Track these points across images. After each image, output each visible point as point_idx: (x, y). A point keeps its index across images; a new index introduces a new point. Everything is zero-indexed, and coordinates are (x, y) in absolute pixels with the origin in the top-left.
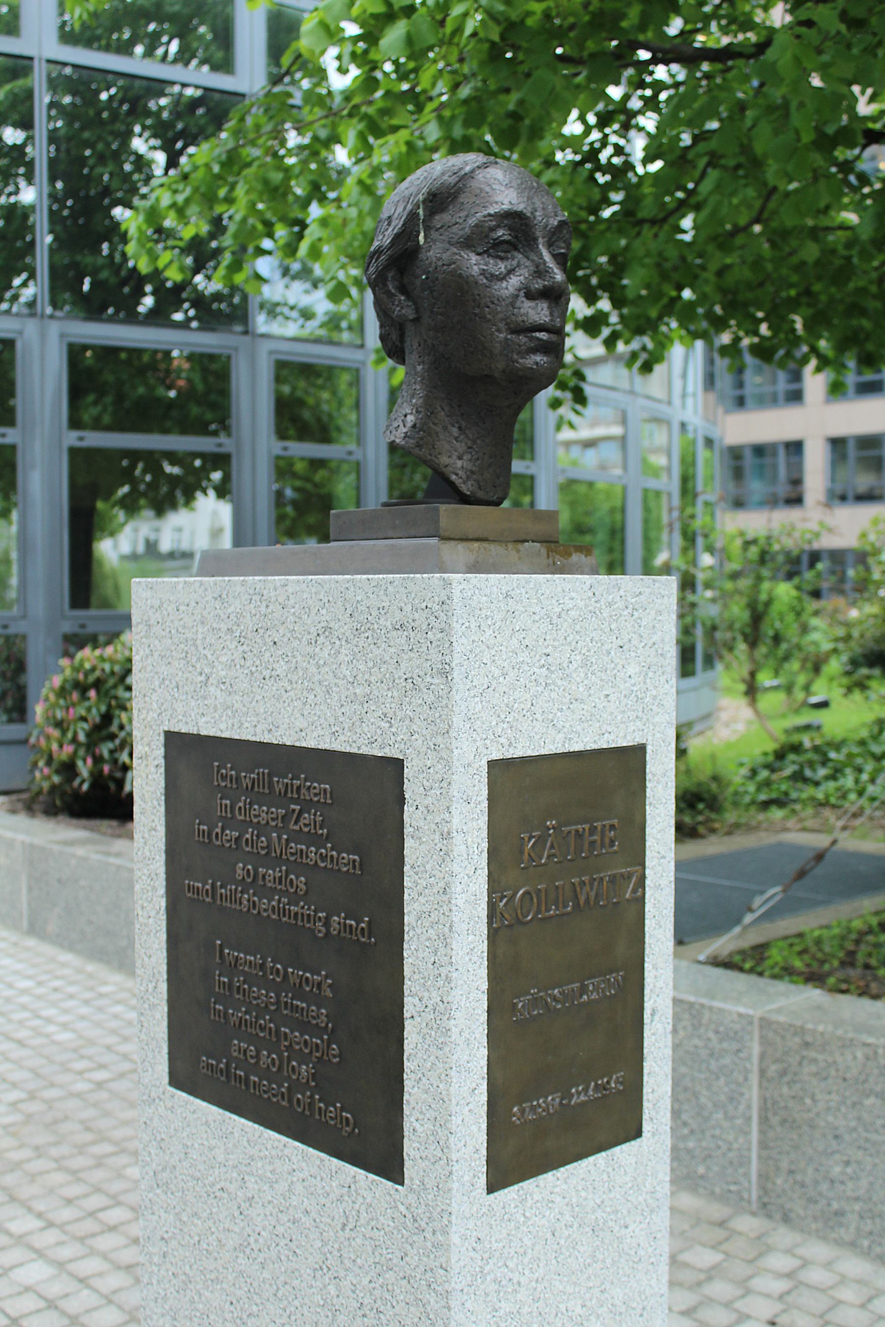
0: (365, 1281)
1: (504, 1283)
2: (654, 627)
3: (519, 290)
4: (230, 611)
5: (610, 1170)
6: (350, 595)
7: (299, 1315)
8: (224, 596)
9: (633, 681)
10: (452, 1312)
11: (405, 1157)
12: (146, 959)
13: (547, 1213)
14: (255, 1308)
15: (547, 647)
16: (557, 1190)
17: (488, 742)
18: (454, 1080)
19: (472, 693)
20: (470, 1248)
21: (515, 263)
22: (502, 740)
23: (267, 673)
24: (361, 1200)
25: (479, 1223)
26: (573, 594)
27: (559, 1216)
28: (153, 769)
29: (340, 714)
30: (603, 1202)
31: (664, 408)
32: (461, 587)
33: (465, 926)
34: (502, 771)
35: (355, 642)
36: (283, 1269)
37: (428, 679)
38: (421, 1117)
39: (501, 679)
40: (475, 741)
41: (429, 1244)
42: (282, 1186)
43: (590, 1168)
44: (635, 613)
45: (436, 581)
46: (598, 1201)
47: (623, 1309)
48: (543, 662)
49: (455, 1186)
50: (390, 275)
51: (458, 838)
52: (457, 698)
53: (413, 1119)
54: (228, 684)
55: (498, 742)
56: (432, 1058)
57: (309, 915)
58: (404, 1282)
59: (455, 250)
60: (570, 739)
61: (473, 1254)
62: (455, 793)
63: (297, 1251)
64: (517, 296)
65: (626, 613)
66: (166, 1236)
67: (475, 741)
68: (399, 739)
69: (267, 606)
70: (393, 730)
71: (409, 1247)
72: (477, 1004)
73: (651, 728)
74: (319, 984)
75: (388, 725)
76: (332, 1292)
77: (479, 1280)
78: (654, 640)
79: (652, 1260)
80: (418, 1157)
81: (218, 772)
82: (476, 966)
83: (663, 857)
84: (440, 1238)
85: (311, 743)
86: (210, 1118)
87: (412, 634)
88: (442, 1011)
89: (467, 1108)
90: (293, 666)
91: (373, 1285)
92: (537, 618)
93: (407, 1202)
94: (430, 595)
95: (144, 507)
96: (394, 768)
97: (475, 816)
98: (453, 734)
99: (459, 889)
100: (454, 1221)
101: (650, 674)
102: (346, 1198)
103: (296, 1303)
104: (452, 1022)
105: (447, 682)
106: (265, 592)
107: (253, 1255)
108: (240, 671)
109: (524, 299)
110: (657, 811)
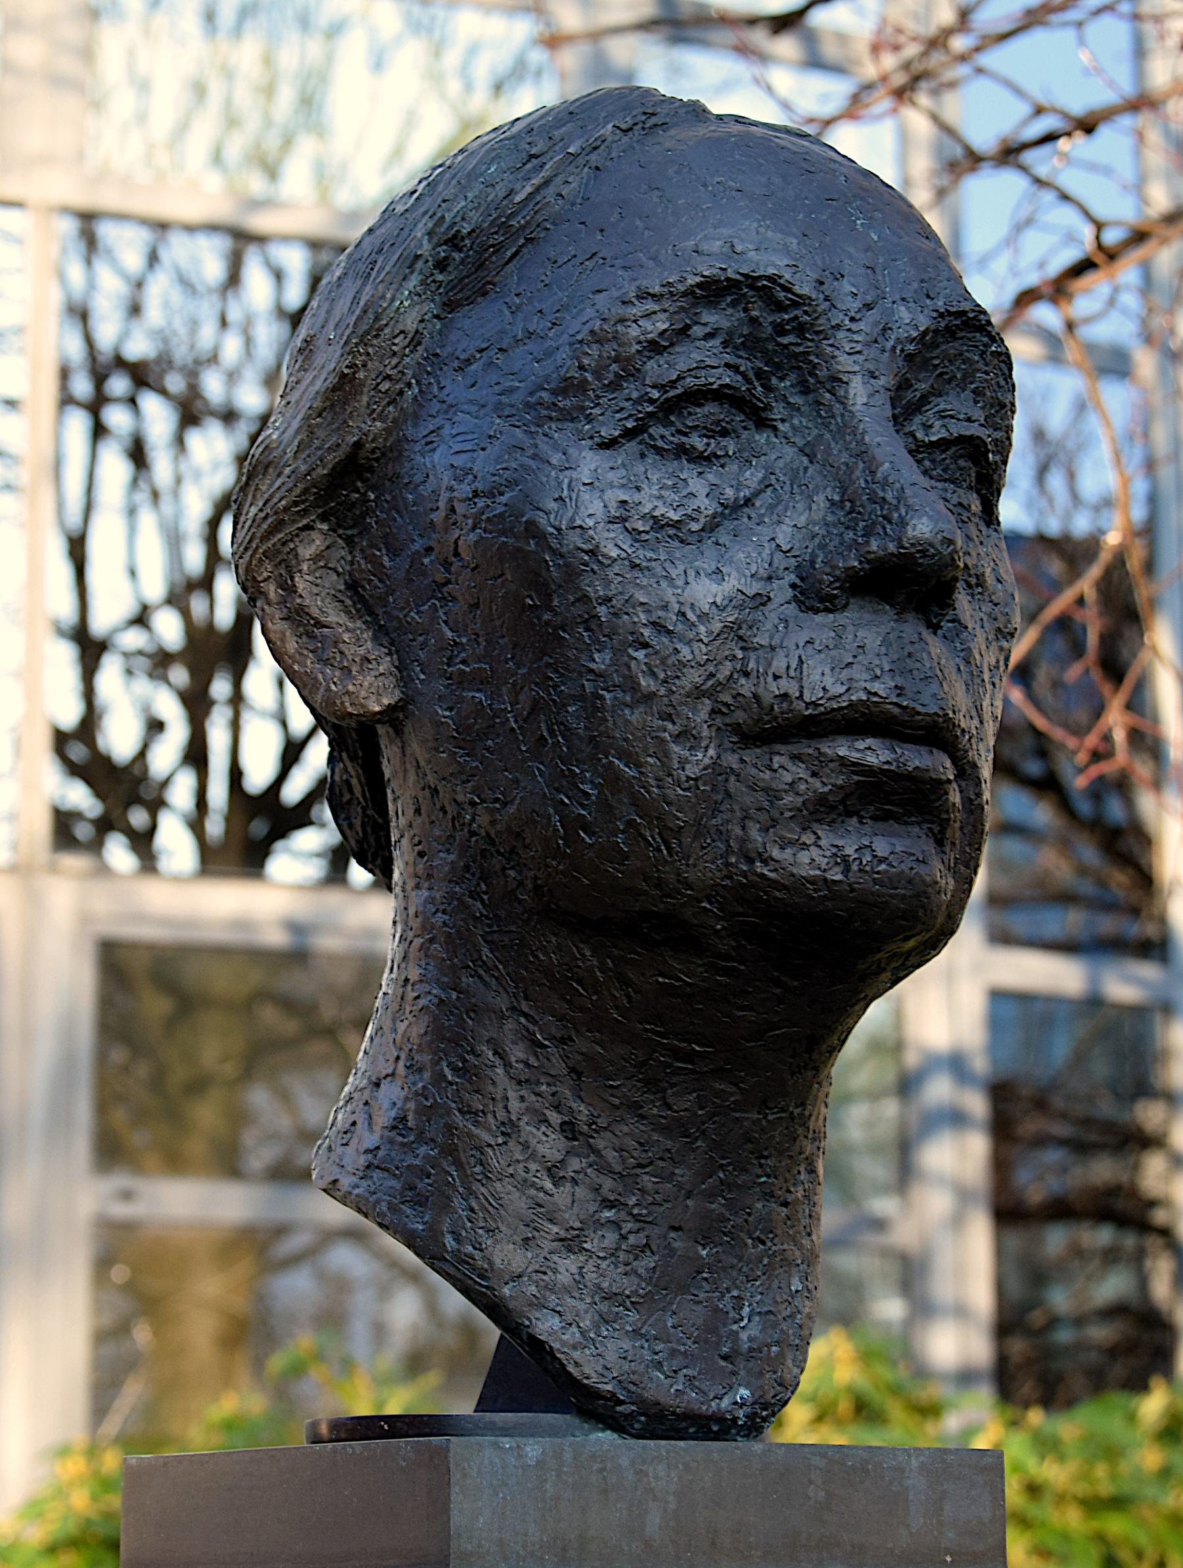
21: (752, 477)
50: (309, 548)
95: (1167, 1122)
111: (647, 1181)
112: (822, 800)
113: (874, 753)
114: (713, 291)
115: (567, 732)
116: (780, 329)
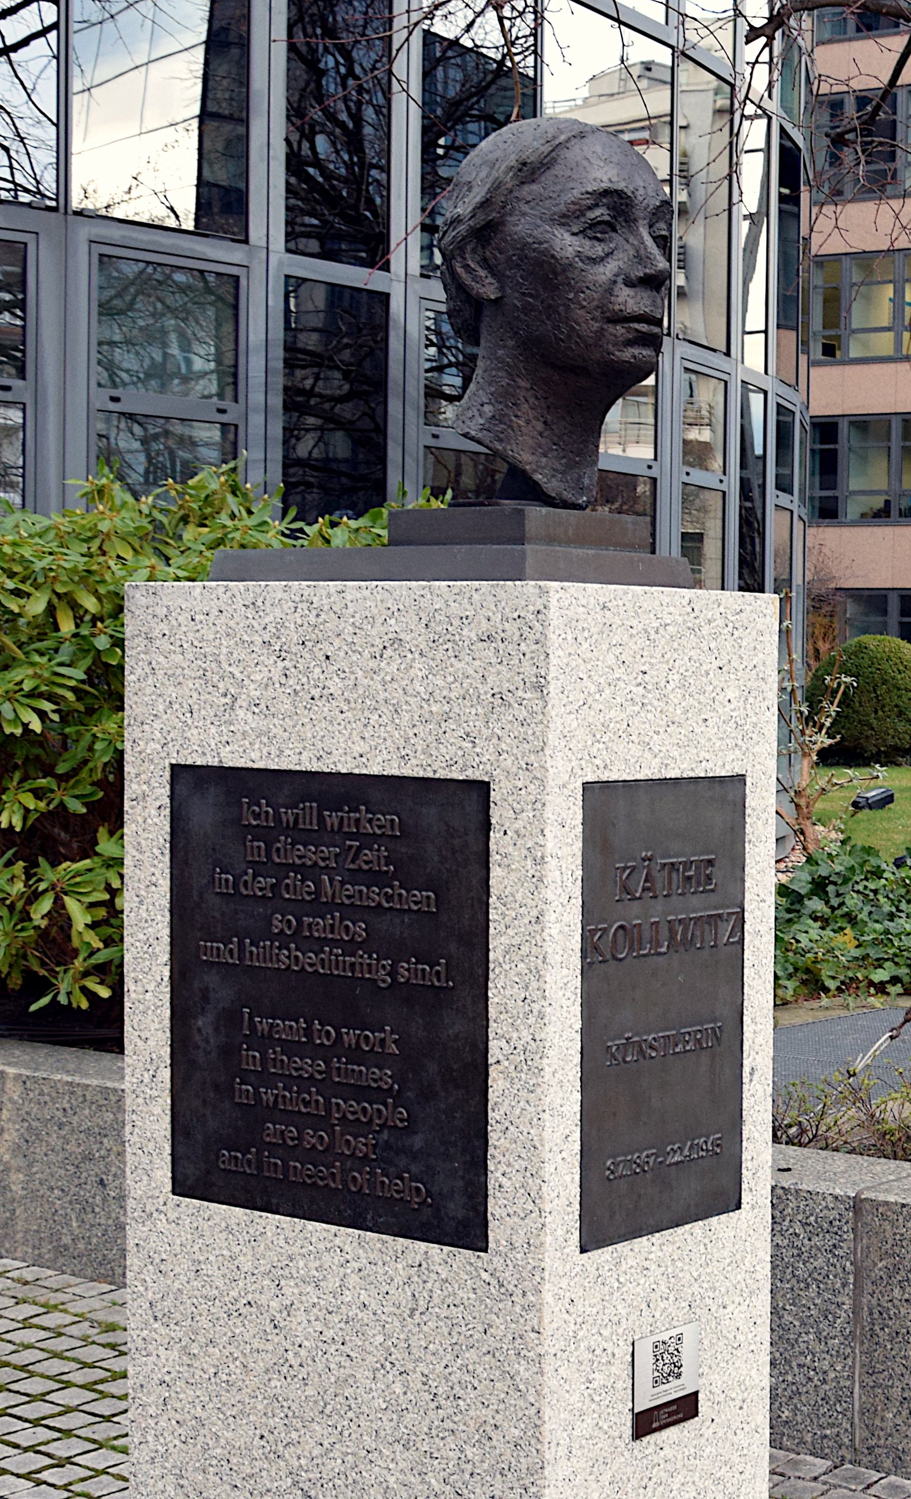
0: (439, 1368)
1: (597, 1352)
2: (755, 648)
3: (616, 275)
4: (267, 620)
5: (707, 1241)
6: (423, 603)
7: (355, 1428)
8: (259, 603)
9: (732, 706)
10: (545, 1378)
11: (490, 1217)
12: (140, 1043)
13: (642, 1281)
14: (294, 1435)
15: (644, 665)
16: (652, 1256)
17: (583, 762)
18: (547, 1124)
19: (569, 708)
20: (564, 1310)
22: (597, 761)
23: (316, 692)
24: (434, 1276)
25: (572, 1284)
26: (672, 609)
27: (654, 1286)
28: (154, 812)
29: (411, 735)
30: (700, 1276)
31: (718, 360)
32: (558, 596)
33: (558, 958)
34: (600, 796)
35: (430, 655)
36: (333, 1379)
37: (520, 693)
38: (508, 1170)
39: (597, 696)
40: (570, 760)
41: (518, 1309)
42: (333, 1283)
43: (686, 1236)
44: (735, 632)
45: (531, 590)
46: (695, 1274)
47: (722, 1398)
48: (639, 680)
49: (549, 1239)
51: (552, 863)
52: (553, 713)
53: (498, 1174)
54: (263, 706)
55: (592, 764)
56: (522, 1104)
57: (369, 965)
58: (488, 1358)
59: (548, 228)
60: (666, 765)
61: (566, 1316)
62: (550, 815)
63: (351, 1354)
64: (615, 282)
65: (726, 631)
66: (167, 1378)
67: (570, 760)
68: (484, 760)
69: (318, 616)
70: (478, 750)
71: (495, 1317)
72: (570, 1044)
73: (751, 758)
74: (383, 1041)
75: (470, 745)
76: (398, 1391)
77: (573, 1346)
78: (755, 662)
79: (752, 1348)
80: (504, 1215)
81: (249, 808)
82: (569, 1003)
83: (763, 901)
84: (532, 1298)
85: (375, 770)
86: (233, 1221)
87: (501, 646)
88: (531, 1058)
89: (560, 1156)
90: (351, 683)
91: (450, 1370)
92: (634, 631)
93: (490, 1268)
94: (524, 603)
96: (481, 790)
97: (570, 840)
98: (548, 751)
99: (553, 917)
100: (547, 1278)
101: (751, 700)
102: (416, 1279)
103: (350, 1414)
104: (545, 1061)
105: (543, 697)
106: (315, 600)
107: (292, 1373)
108: (280, 690)
109: (622, 286)
110: (757, 850)
111: (565, 438)
112: (630, 340)
113: (643, 327)
114: (606, 193)
115: (559, 314)
116: (621, 204)
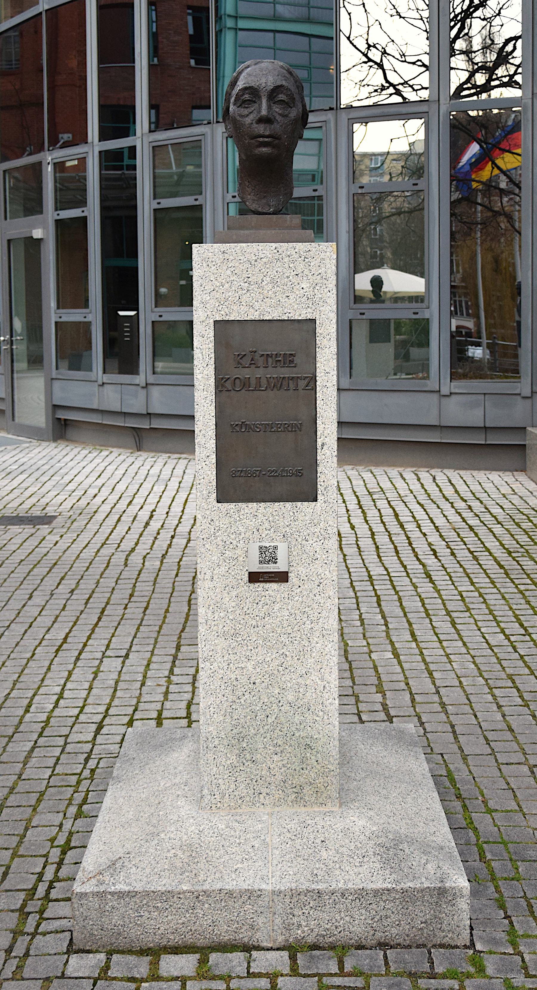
19: (205, 292)
78: (320, 272)
